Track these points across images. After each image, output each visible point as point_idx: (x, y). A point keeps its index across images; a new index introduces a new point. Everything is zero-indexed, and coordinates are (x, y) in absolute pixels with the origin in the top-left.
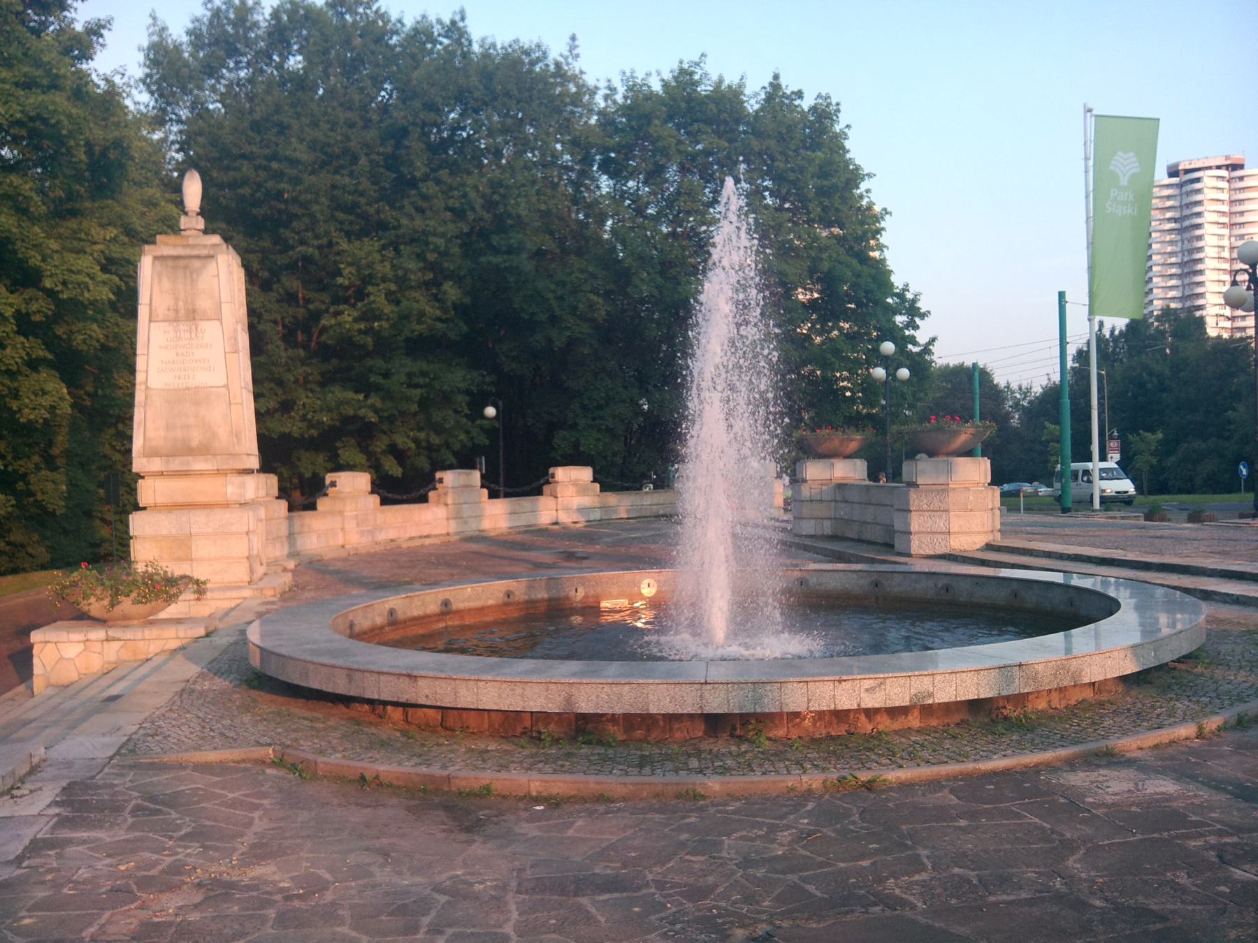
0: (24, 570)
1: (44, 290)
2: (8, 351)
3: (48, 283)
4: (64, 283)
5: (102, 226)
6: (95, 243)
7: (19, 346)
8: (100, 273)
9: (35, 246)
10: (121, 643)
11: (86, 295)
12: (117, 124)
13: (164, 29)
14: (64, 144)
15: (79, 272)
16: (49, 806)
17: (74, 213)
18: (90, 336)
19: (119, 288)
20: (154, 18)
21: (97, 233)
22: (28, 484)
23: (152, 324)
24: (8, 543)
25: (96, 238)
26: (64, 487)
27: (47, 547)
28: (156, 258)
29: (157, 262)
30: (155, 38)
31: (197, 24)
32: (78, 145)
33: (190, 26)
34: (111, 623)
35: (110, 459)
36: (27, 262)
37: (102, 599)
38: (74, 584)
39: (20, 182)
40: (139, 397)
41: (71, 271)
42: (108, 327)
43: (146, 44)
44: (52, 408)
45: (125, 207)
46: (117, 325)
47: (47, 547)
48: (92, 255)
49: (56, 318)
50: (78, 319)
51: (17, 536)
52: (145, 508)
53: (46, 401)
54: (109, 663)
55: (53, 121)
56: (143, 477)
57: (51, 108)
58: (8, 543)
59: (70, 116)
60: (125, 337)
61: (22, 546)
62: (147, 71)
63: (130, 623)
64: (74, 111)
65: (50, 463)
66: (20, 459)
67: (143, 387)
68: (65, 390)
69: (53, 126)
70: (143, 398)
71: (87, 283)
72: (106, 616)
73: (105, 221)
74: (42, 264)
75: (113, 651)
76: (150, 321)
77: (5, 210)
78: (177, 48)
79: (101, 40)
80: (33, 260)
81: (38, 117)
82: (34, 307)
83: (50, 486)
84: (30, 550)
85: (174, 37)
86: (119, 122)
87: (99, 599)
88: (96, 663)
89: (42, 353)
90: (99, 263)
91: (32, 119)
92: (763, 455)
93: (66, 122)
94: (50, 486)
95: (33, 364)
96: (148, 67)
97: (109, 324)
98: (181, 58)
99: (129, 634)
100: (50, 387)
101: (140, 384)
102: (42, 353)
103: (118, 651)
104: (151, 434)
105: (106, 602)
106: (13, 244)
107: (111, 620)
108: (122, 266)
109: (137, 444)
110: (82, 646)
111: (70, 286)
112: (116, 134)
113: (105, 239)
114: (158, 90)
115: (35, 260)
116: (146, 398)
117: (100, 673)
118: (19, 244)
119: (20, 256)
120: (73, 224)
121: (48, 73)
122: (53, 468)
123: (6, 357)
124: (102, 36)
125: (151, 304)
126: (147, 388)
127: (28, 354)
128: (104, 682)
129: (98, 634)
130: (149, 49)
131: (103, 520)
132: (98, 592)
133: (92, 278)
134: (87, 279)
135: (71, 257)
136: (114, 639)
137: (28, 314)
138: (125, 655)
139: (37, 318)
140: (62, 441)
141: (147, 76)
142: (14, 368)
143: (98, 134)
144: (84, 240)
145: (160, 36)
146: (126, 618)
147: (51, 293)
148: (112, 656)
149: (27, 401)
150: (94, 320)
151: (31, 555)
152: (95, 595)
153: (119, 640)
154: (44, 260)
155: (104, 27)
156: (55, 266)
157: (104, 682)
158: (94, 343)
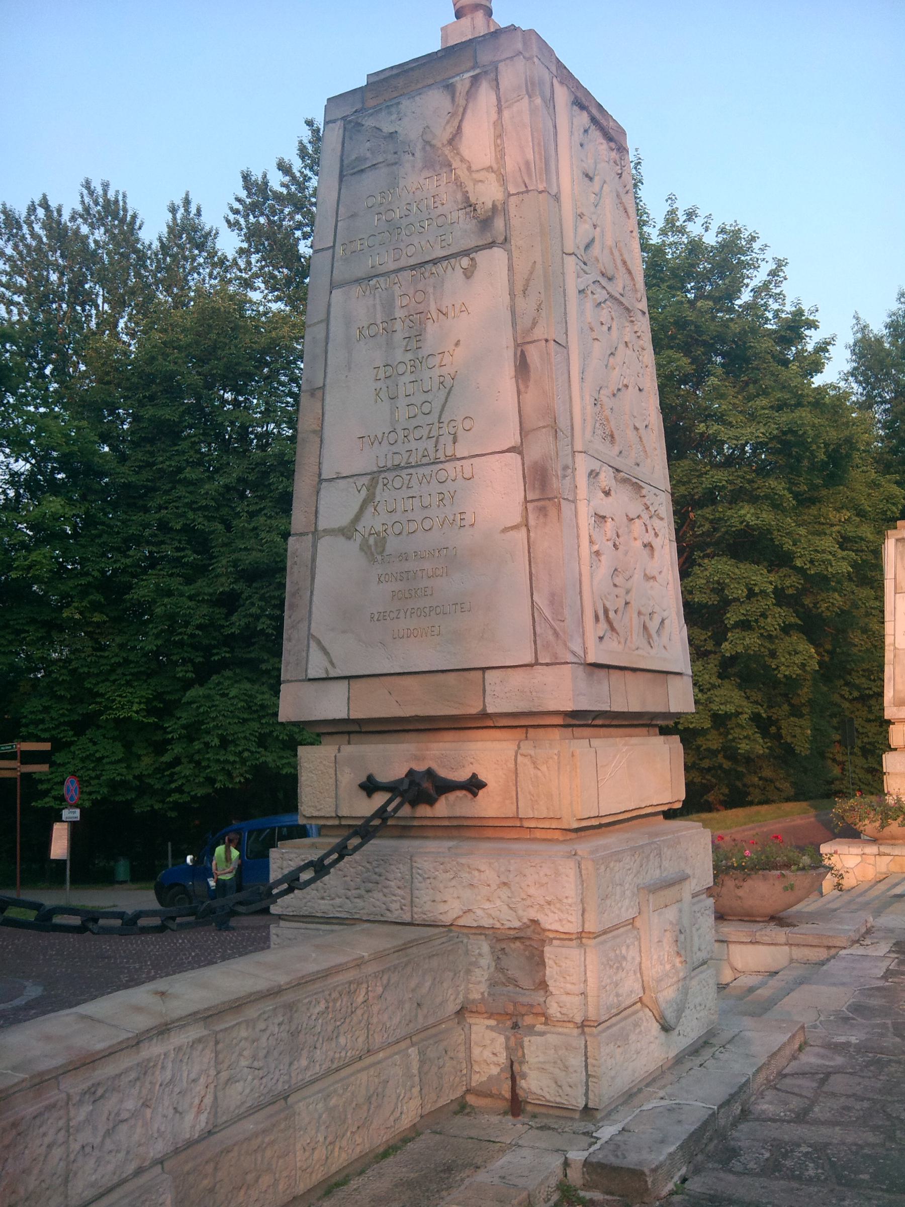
0: (773, 801)
1: (795, 568)
2: (769, 620)
3: (798, 563)
4: (812, 562)
5: (838, 510)
6: (832, 525)
7: (777, 615)
8: (839, 551)
9: (787, 534)
10: (890, 858)
11: (830, 570)
12: (847, 424)
13: (866, 327)
14: (808, 449)
15: (823, 551)
16: (889, 952)
17: (813, 501)
18: (832, 603)
19: (855, 561)
20: (857, 319)
21: (833, 516)
22: (779, 728)
23: (898, 595)
24: (760, 779)
25: (835, 520)
26: (809, 732)
27: (792, 782)
28: (897, 540)
29: (899, 544)
30: (859, 335)
31: (894, 318)
32: (819, 447)
33: (888, 320)
34: (880, 842)
35: (840, 706)
36: (782, 548)
37: (875, 821)
38: (852, 809)
39: (776, 483)
40: (889, 656)
41: (816, 551)
42: (845, 595)
43: (851, 342)
44: (803, 666)
45: (853, 490)
46: (853, 593)
47: (792, 782)
48: (831, 535)
49: (803, 591)
50: (821, 589)
51: (767, 773)
52: (896, 749)
53: (798, 659)
54: (881, 873)
55: (800, 433)
56: (894, 723)
57: (799, 422)
58: (760, 779)
59: (814, 426)
60: (860, 603)
61: (772, 781)
62: (855, 365)
63: (897, 842)
64: (816, 421)
65: (796, 712)
66: (772, 707)
67: (892, 648)
68: (813, 650)
69: (800, 436)
70: (892, 657)
71: (830, 560)
72: (877, 835)
73: (838, 504)
74: (794, 548)
75: (883, 864)
76: (895, 593)
77: (766, 507)
78: (879, 341)
79: (827, 354)
80: (786, 545)
81: (791, 431)
82: (788, 583)
83: (798, 731)
84: (778, 784)
85: (875, 332)
86: (848, 422)
87: (872, 821)
88: (870, 874)
89: (794, 620)
90: (838, 543)
91: (784, 433)
92: (534, 694)
93: (810, 432)
94: (798, 731)
95: (786, 629)
96: (855, 361)
97: (845, 592)
98: (883, 349)
99: (897, 851)
100: (801, 648)
101: (890, 644)
102: (794, 620)
103: (888, 864)
104: (899, 687)
105: (877, 824)
106: (772, 533)
107: (882, 839)
108: (856, 542)
109: (889, 695)
110: (859, 859)
111: (817, 564)
112: (847, 433)
113: (840, 521)
114: (865, 380)
115: (788, 545)
116: (895, 656)
117: (873, 881)
118: (776, 533)
119: (777, 543)
120: (813, 511)
121: (795, 395)
122: (801, 716)
123: (767, 625)
124: (828, 351)
125: (895, 578)
126: (895, 648)
127: (784, 622)
128: (882, 887)
129: (872, 849)
130: (855, 345)
131: (834, 760)
132: (871, 816)
133: (834, 555)
134: (830, 557)
135: (816, 540)
136: (885, 855)
137: (783, 588)
138: (894, 868)
139: (790, 591)
140: (805, 693)
141: (855, 369)
142: (774, 633)
143: (833, 435)
144: (823, 524)
145: (863, 333)
146: (894, 838)
147: (801, 571)
148: (883, 869)
149: (783, 660)
150: (835, 590)
151: (778, 789)
152: (869, 818)
153: (889, 855)
154: (794, 545)
155: (828, 344)
156: (804, 548)
157: (882, 887)
158: (836, 609)
